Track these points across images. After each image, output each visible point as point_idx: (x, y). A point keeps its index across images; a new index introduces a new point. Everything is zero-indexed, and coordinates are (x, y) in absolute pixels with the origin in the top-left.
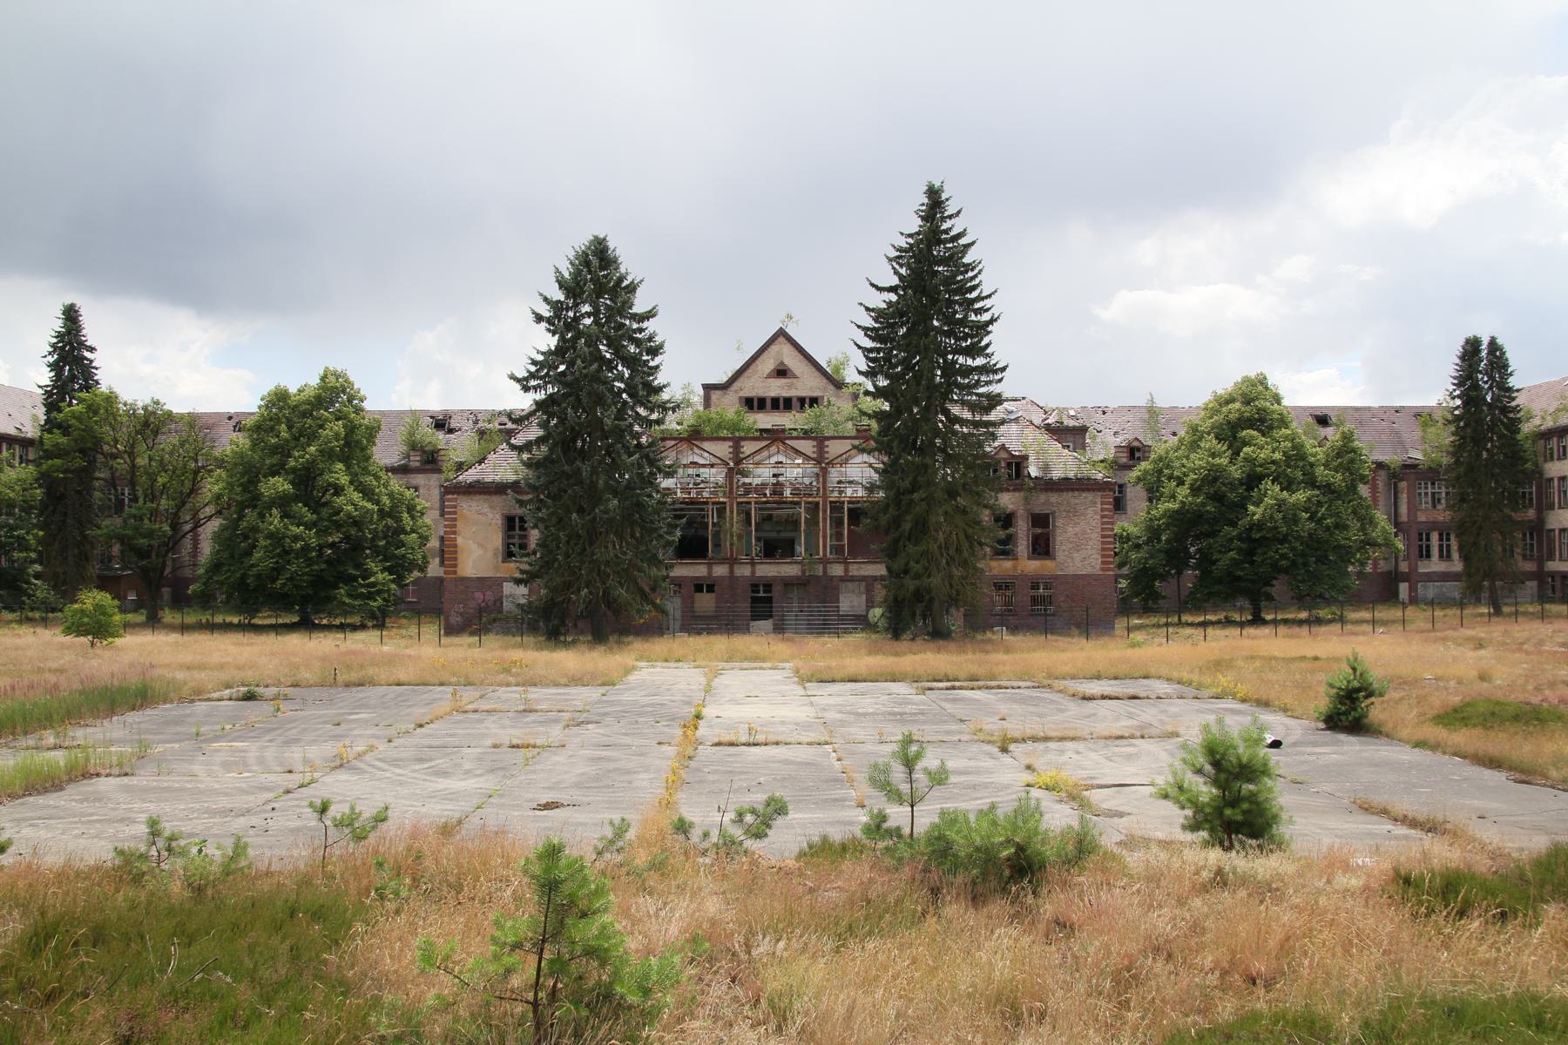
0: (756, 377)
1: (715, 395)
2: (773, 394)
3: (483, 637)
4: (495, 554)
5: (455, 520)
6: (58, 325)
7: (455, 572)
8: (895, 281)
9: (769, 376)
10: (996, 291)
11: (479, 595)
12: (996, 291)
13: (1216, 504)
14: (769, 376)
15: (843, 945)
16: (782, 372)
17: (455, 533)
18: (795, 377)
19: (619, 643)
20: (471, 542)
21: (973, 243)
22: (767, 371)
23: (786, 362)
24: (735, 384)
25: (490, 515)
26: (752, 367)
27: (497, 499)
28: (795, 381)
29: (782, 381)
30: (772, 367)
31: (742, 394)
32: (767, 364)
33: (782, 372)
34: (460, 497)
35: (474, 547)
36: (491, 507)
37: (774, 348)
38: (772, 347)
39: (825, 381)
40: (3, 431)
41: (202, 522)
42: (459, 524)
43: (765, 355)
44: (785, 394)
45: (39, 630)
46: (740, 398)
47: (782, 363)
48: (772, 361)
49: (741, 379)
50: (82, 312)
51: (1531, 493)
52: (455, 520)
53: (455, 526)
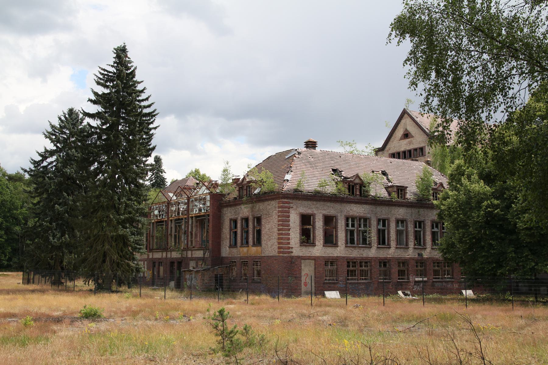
0: (395, 140)
2: (402, 149)
9: (401, 139)
10: (159, 126)
12: (159, 126)
13: (28, 181)
14: (401, 139)
15: (223, 348)
16: (406, 135)
22: (400, 136)
26: (394, 135)
29: (407, 141)
32: (400, 132)
40: (540, 311)
41: (473, 328)
44: (408, 148)
45: (44, 310)
46: (389, 154)
47: (406, 130)
49: (390, 143)
50: (163, 161)
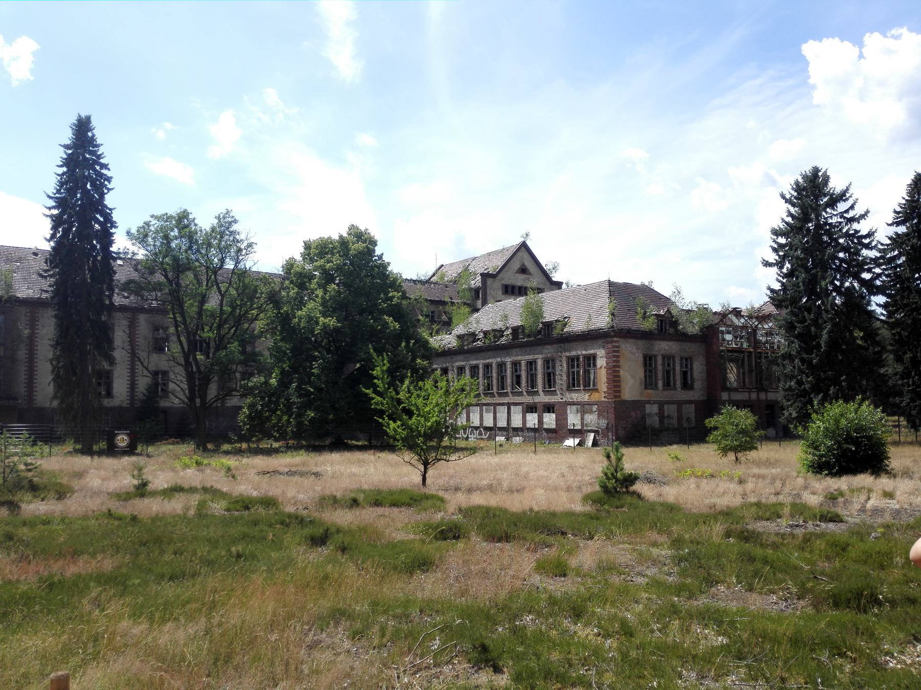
1: (489, 281)
3: (781, 443)
4: (641, 383)
5: (618, 357)
6: (67, 136)
7: (620, 397)
8: (54, 204)
11: (633, 414)
16: (523, 270)
17: (619, 367)
18: (530, 274)
19: (276, 457)
20: (627, 374)
21: (112, 189)
23: (526, 264)
24: (499, 275)
25: (637, 354)
27: (641, 343)
28: (530, 276)
29: (523, 276)
30: (519, 266)
31: (503, 282)
32: (516, 265)
33: (523, 270)
34: (621, 340)
35: (629, 377)
36: (637, 349)
37: (519, 254)
38: (519, 253)
39: (545, 279)
42: (621, 359)
43: (514, 259)
47: (524, 264)
48: (518, 262)
51: (578, 372)
52: (618, 357)
53: (618, 361)
